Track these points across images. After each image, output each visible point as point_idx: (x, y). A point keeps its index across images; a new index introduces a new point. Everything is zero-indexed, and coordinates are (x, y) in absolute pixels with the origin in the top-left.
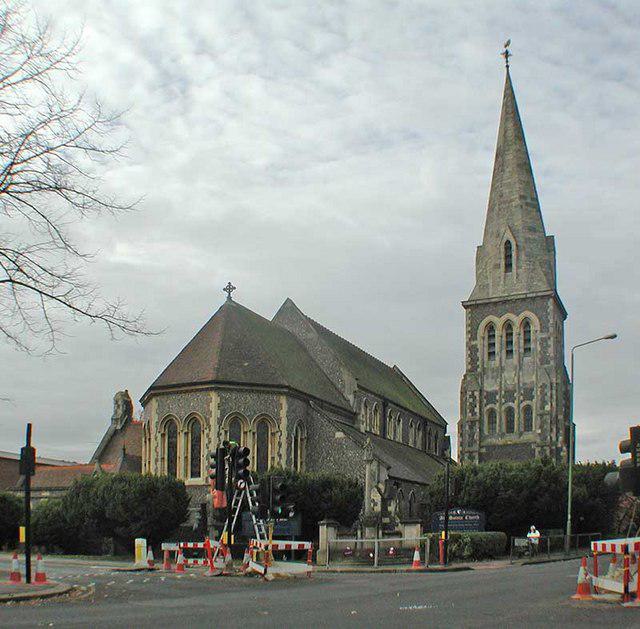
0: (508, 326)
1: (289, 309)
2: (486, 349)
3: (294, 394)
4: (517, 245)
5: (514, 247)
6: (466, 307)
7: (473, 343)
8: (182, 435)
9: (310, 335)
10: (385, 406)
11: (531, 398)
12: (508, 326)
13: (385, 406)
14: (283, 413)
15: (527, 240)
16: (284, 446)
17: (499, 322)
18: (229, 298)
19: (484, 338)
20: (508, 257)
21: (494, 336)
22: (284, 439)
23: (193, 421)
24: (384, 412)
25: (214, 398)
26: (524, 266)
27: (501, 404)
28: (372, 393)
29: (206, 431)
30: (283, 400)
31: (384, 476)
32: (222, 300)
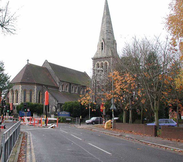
1: (46, 62)
3: (38, 84)
4: (104, 43)
5: (103, 44)
6: (93, 59)
7: (94, 68)
10: (70, 85)
13: (70, 85)
14: (35, 89)
15: (107, 42)
16: (35, 96)
18: (28, 63)
19: (96, 67)
22: (35, 95)
25: (20, 86)
26: (106, 49)
28: (65, 82)
30: (35, 86)
31: (57, 103)
32: (26, 63)
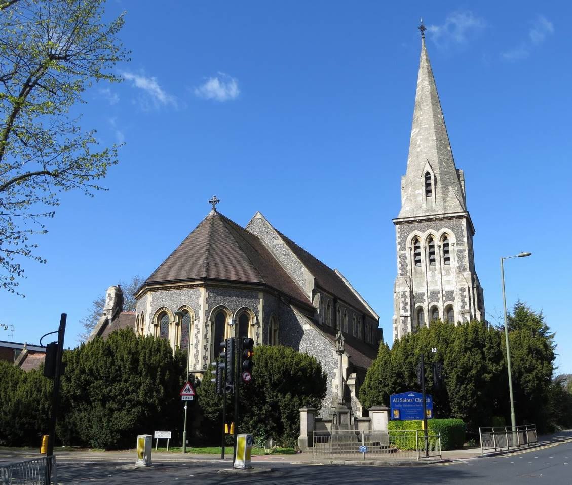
0: (430, 239)
2: (413, 258)
7: (403, 252)
8: (174, 325)
9: (276, 242)
11: (453, 299)
12: (430, 239)
17: (423, 237)
20: (428, 185)
21: (419, 246)
23: (183, 314)
24: (335, 308)
27: (444, 302)
29: (196, 322)
